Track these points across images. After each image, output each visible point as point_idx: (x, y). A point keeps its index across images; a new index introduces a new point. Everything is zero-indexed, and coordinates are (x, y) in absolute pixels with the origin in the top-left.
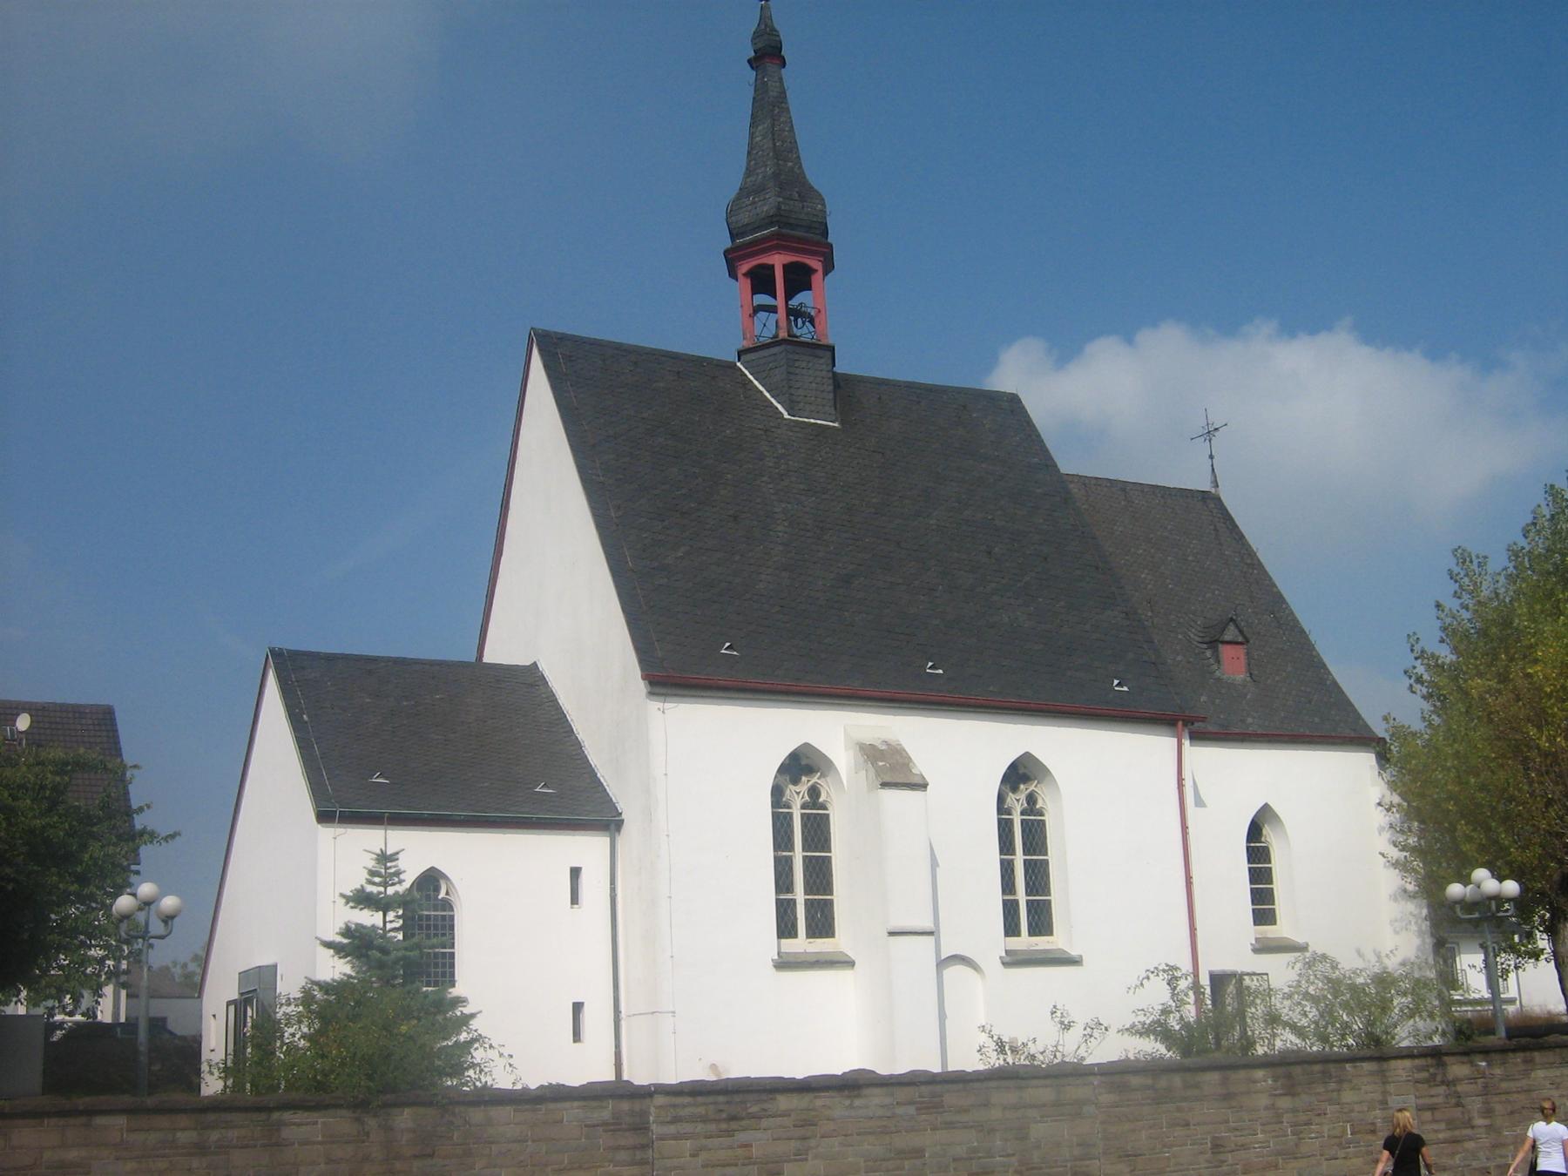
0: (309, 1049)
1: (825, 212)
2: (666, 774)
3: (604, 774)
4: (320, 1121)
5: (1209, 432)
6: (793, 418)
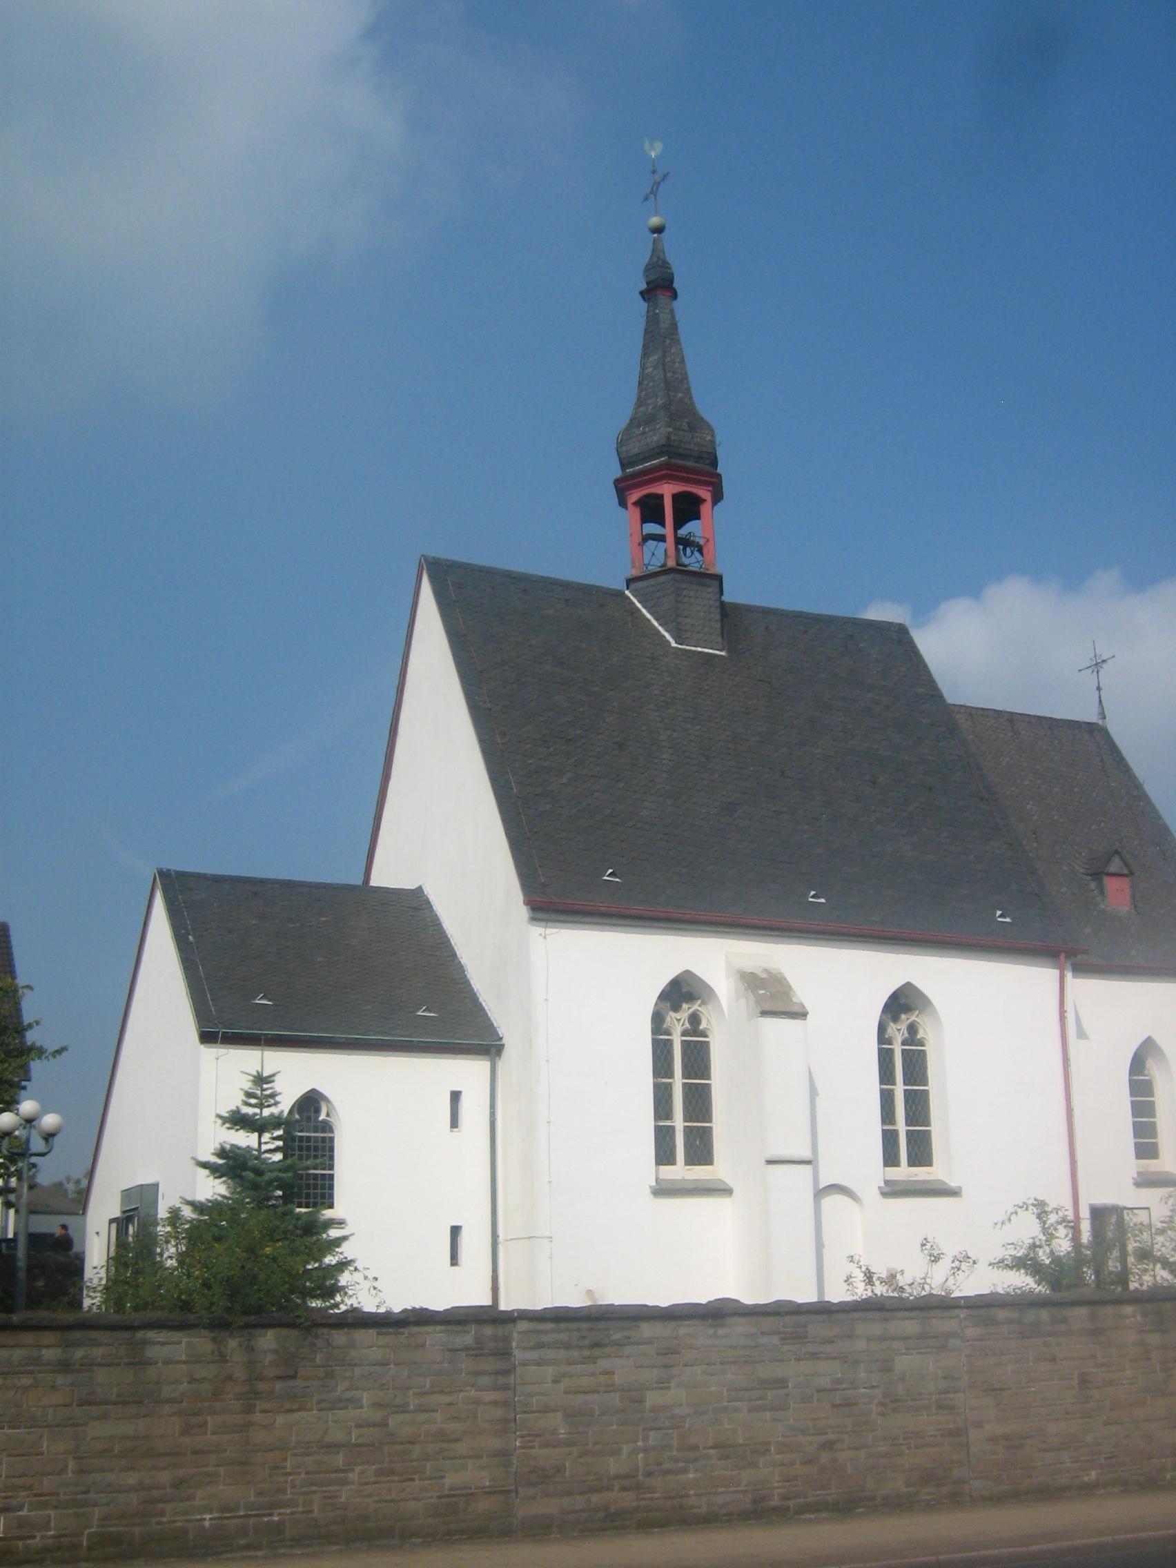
0: (176, 1269)
1: (715, 442)
2: (546, 1000)
3: (487, 999)
4: (185, 1340)
5: (1097, 664)
6: (680, 646)
